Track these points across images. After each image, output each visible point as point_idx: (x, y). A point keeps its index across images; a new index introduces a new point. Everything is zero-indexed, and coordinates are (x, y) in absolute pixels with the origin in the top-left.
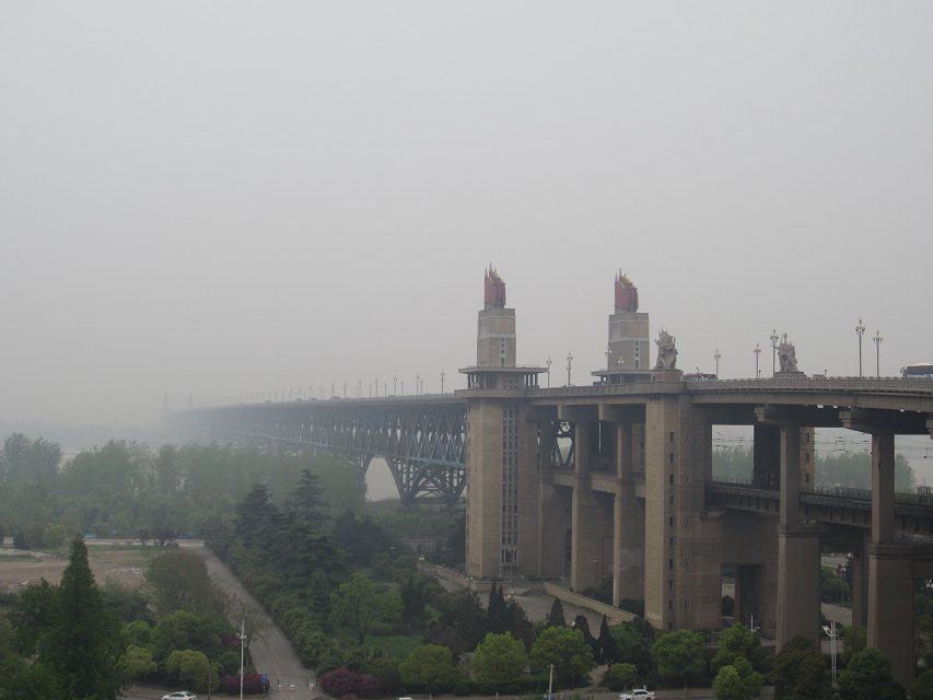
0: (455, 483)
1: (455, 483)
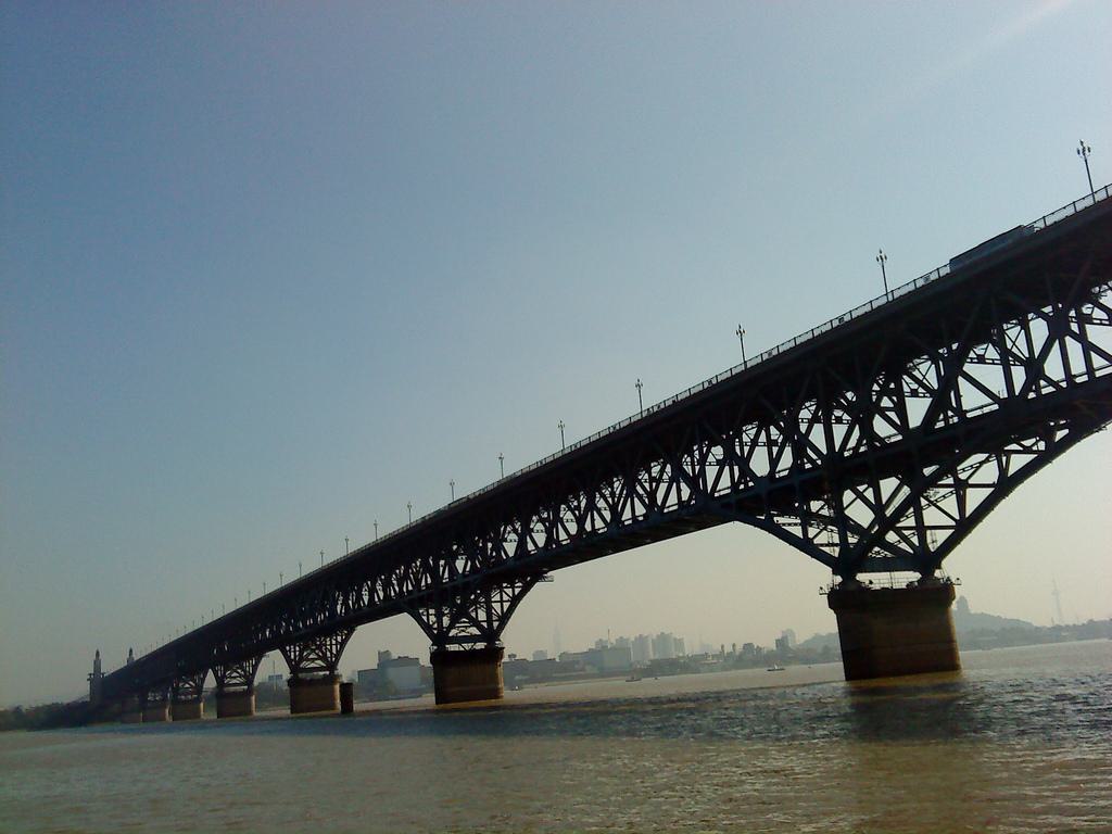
0: (334, 652)
1: (334, 652)
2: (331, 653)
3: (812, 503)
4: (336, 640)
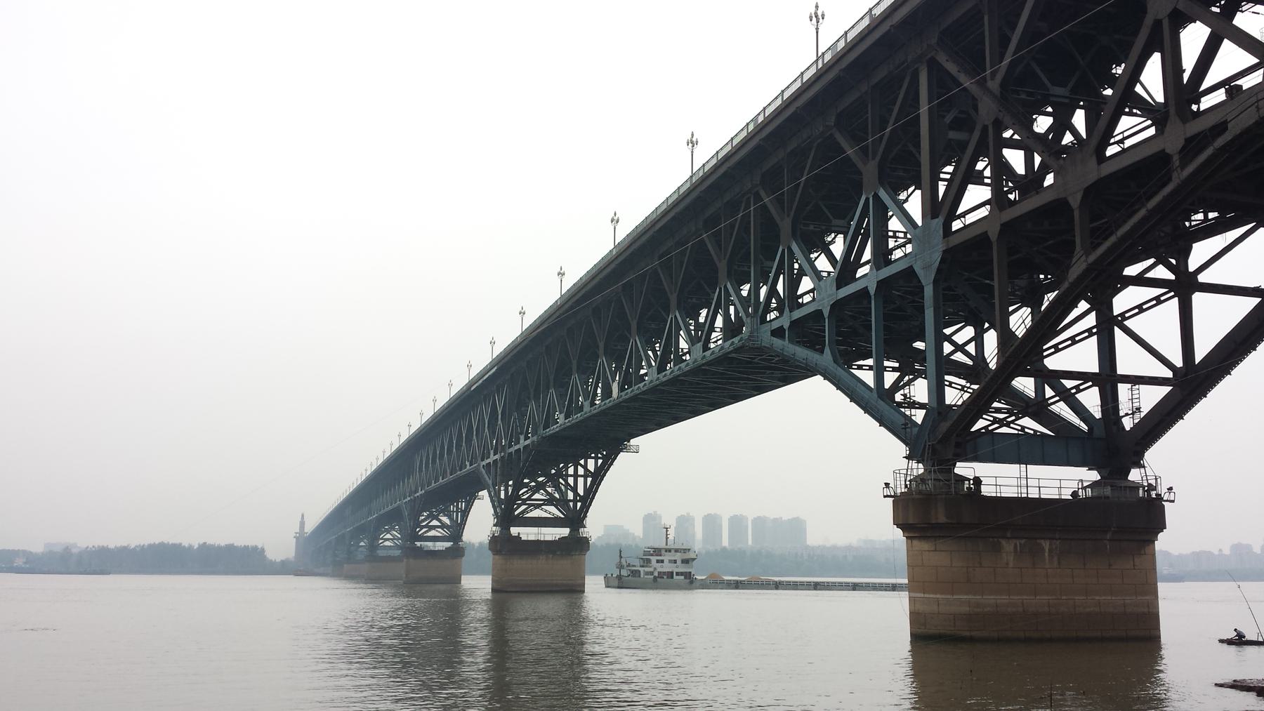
0: (581, 491)
1: (581, 491)
4: (585, 467)
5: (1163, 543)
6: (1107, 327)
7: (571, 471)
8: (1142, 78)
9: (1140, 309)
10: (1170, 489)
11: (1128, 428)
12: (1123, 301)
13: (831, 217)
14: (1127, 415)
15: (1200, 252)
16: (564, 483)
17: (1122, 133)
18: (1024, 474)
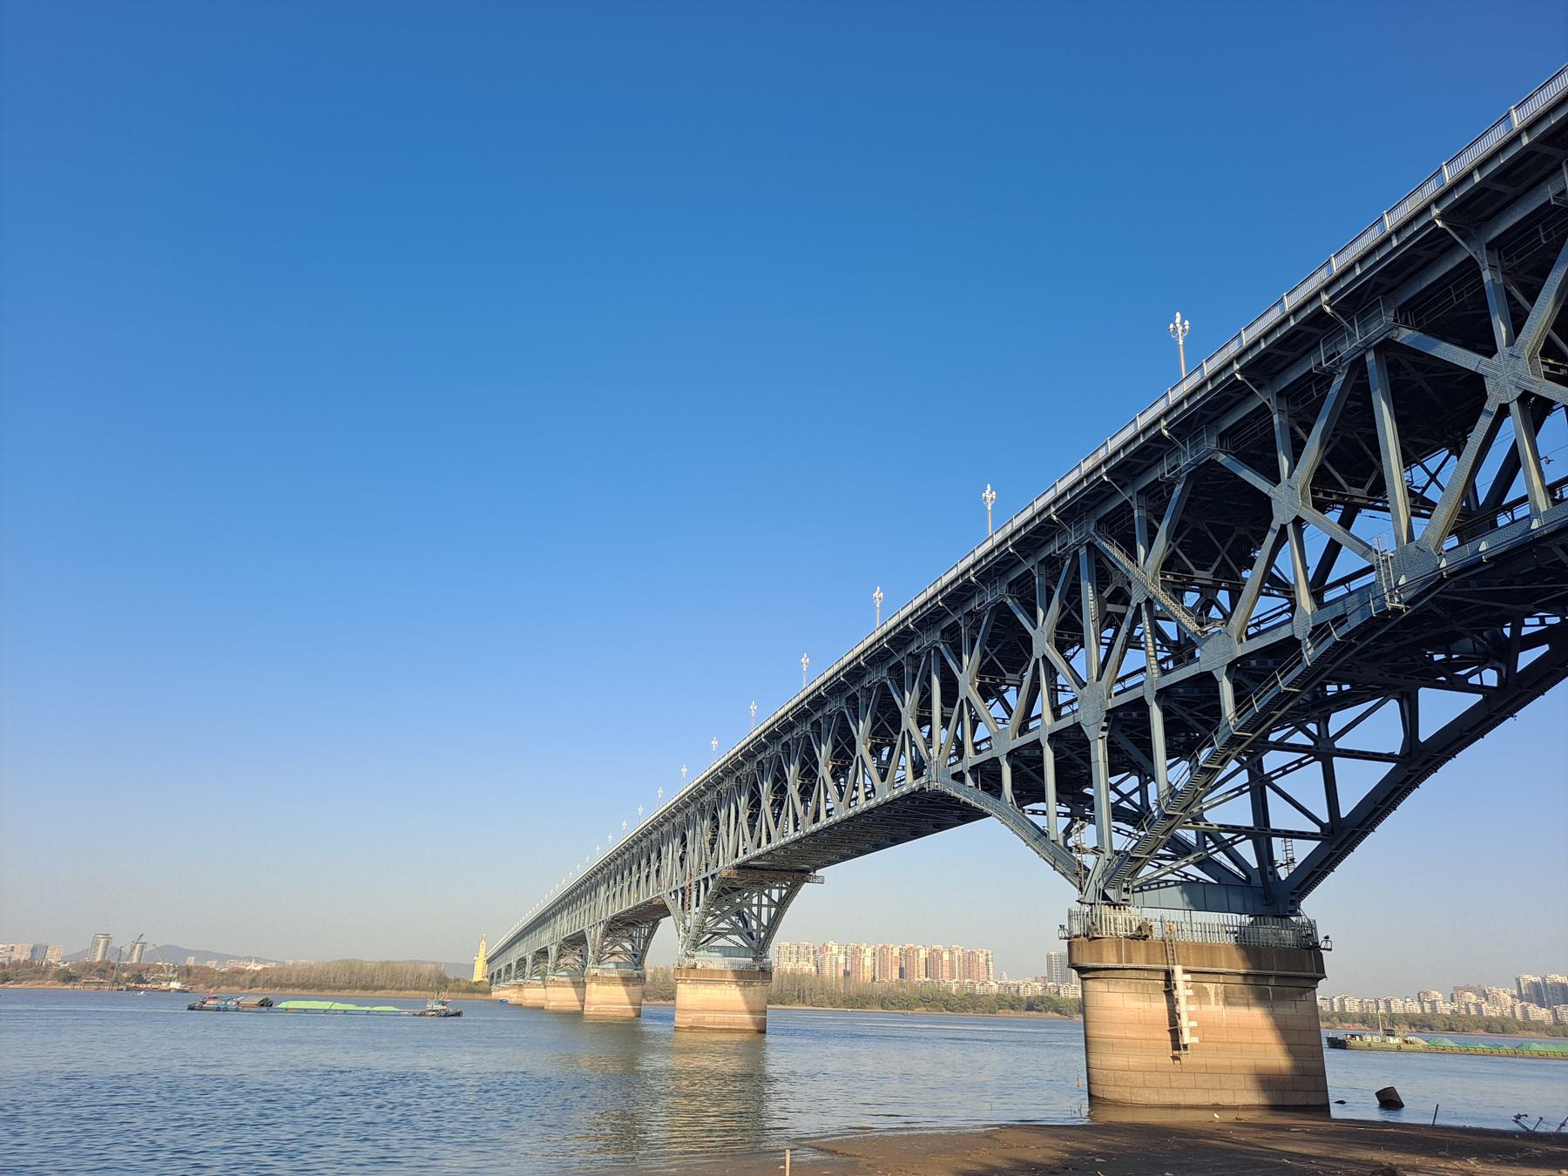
1: (764, 921)
2: (760, 924)
3: (1250, 841)
4: (769, 897)
5: (1323, 990)
6: (1259, 785)
7: (755, 901)
8: (1276, 563)
9: (1284, 770)
10: (1327, 938)
11: (1283, 878)
12: (1272, 761)
13: (1006, 672)
14: (1282, 865)
15: (1337, 721)
16: (747, 911)
17: (1258, 617)
18: (1188, 919)
